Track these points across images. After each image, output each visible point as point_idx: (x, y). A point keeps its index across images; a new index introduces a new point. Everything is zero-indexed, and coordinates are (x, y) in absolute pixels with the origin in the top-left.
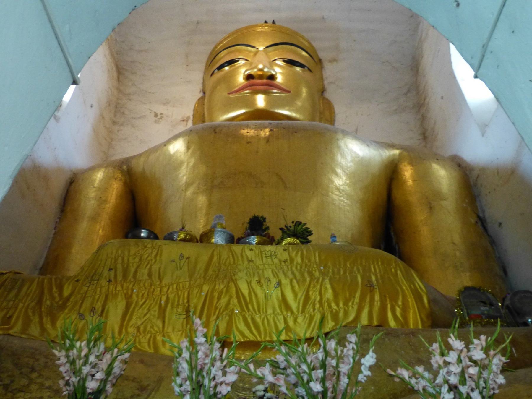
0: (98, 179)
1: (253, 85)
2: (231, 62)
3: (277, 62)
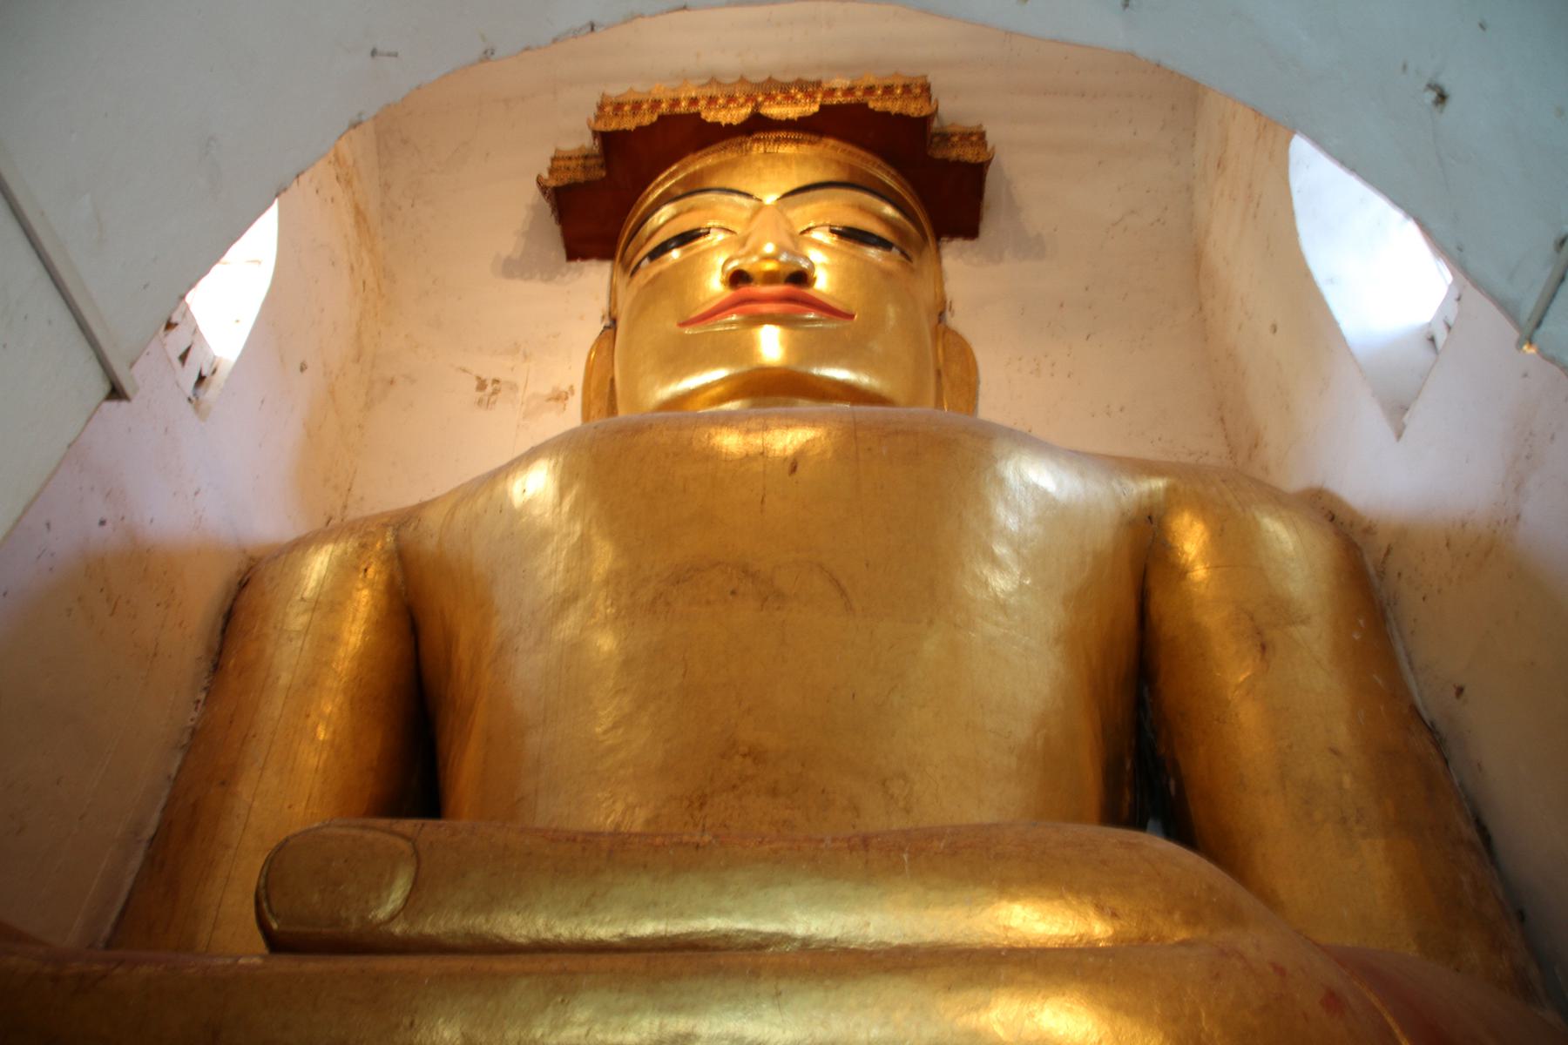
2: (686, 238)
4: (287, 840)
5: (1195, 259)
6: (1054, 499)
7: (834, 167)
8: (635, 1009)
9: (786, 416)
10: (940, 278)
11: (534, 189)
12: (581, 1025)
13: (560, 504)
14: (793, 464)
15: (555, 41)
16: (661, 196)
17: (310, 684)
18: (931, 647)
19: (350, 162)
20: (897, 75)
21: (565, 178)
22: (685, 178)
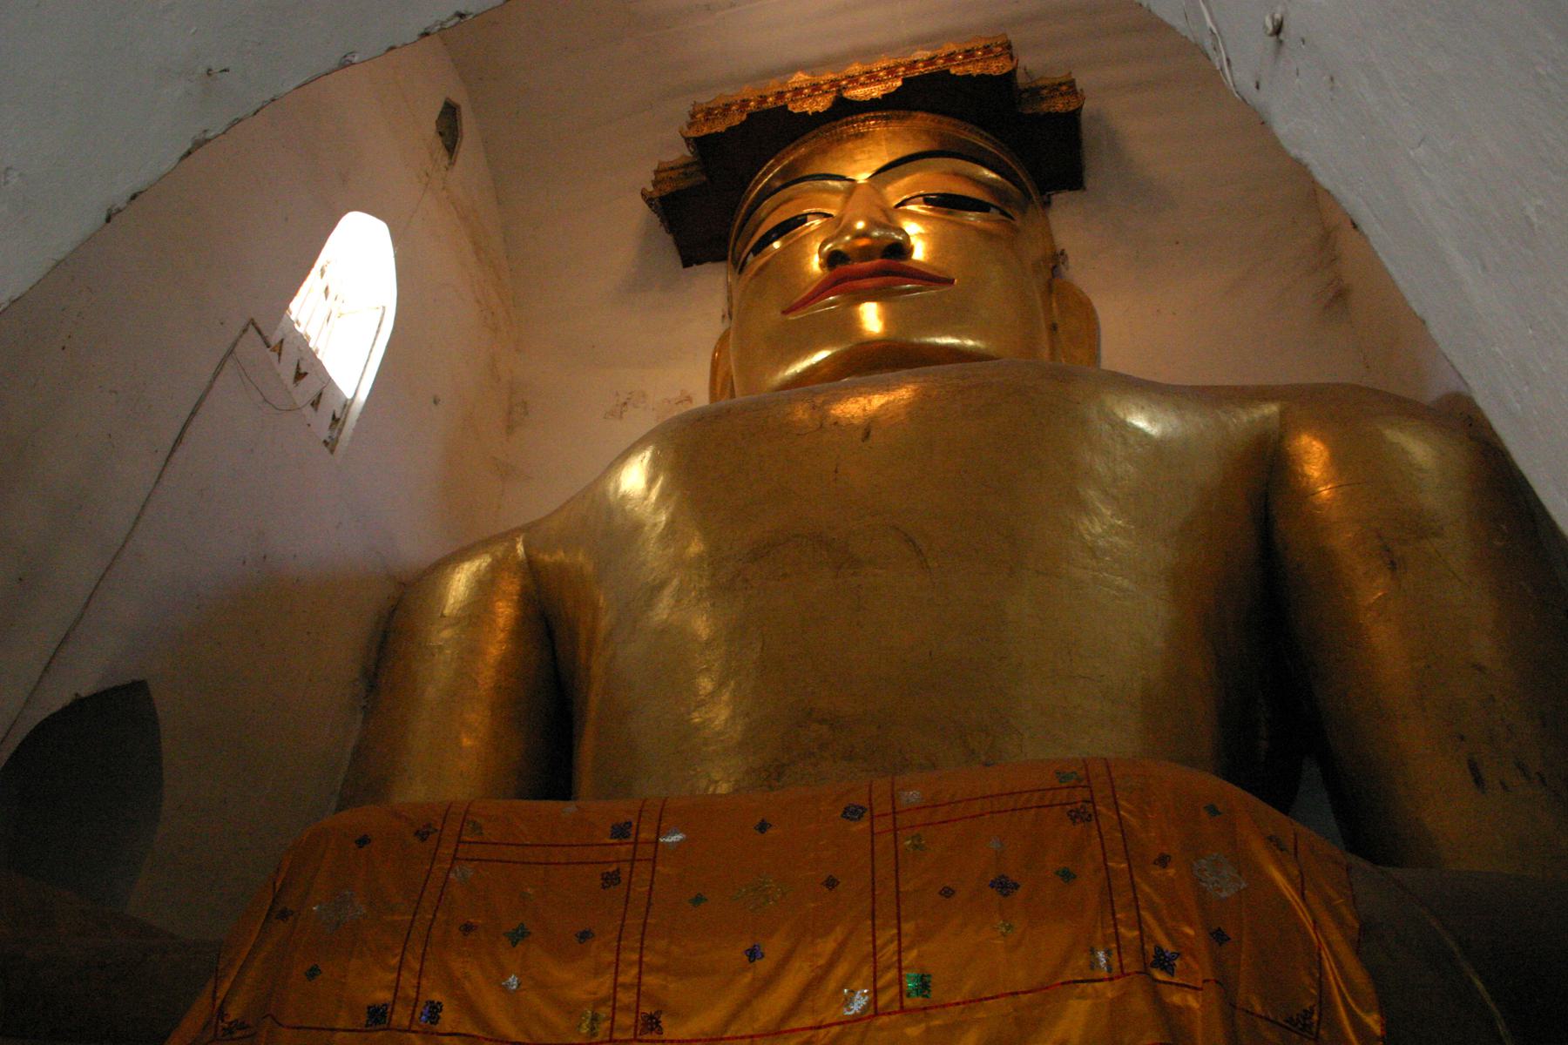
1: (844, 280)
21: (668, 189)
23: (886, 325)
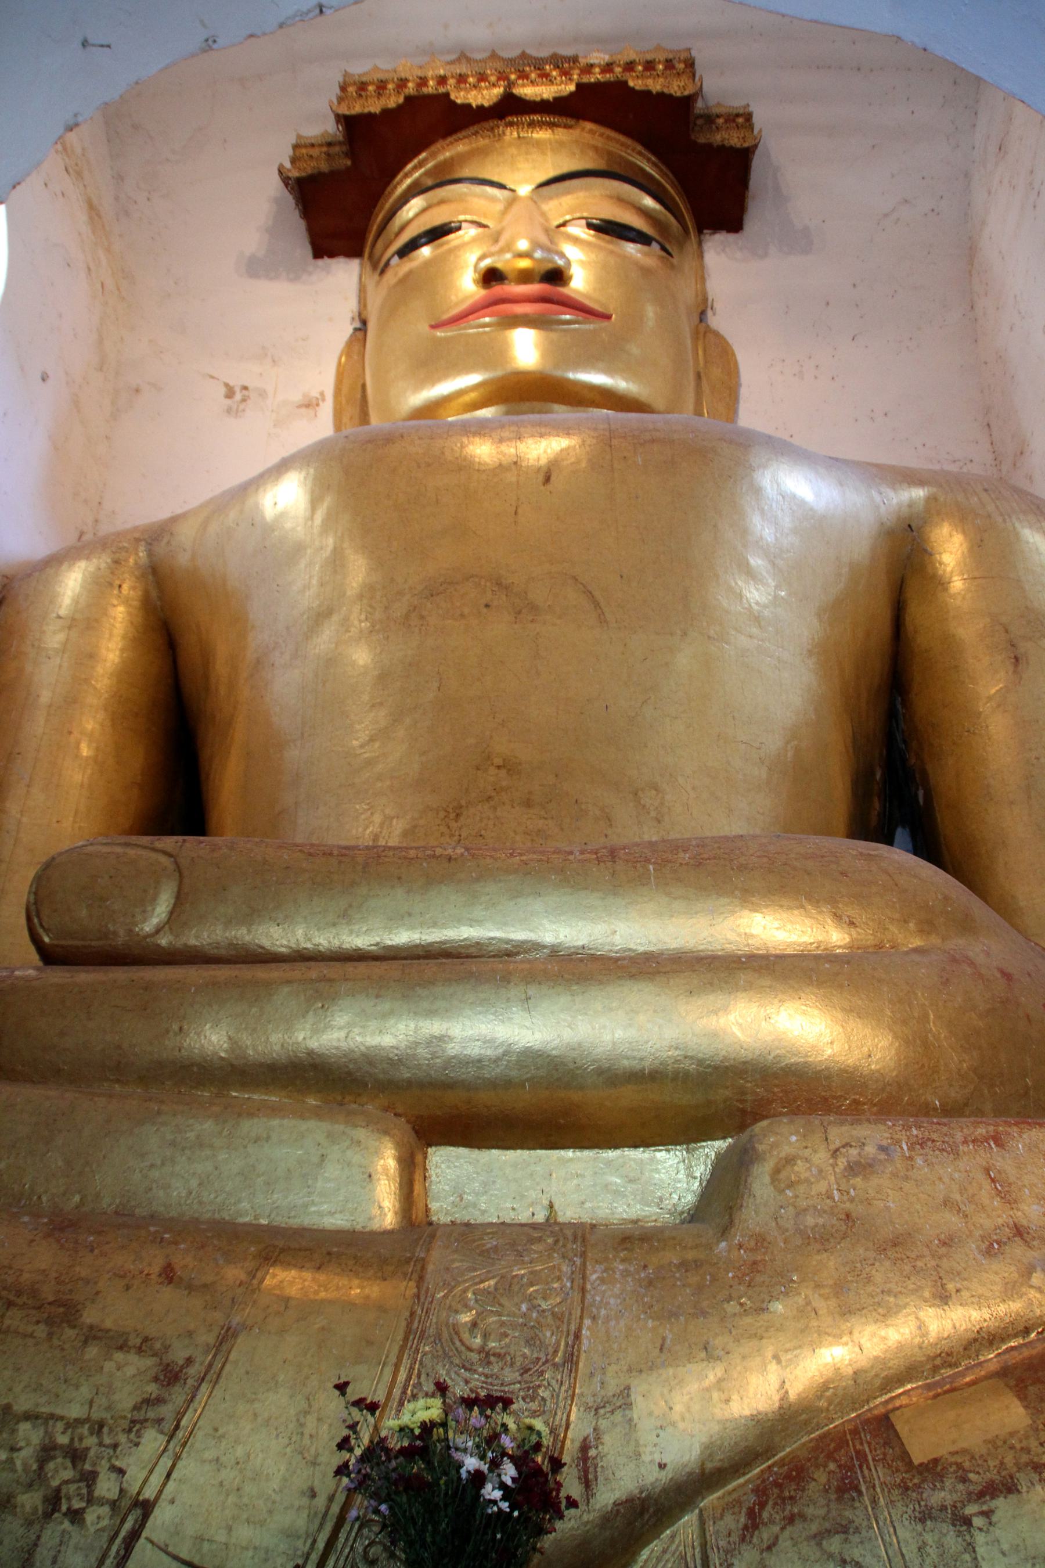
0: (69, 593)
2: (437, 233)
3: (571, 229)
4: (53, 858)
5: (969, 253)
6: (811, 509)
7: (591, 153)
8: (391, 1013)
9: (540, 424)
10: (701, 277)
11: (276, 181)
12: (340, 1028)
13: (312, 518)
14: (547, 475)
15: (281, 26)
16: (410, 188)
17: (72, 700)
18: (684, 660)
19: (79, 151)
20: (658, 48)
21: (308, 168)
22: (435, 167)
23: (544, 355)
